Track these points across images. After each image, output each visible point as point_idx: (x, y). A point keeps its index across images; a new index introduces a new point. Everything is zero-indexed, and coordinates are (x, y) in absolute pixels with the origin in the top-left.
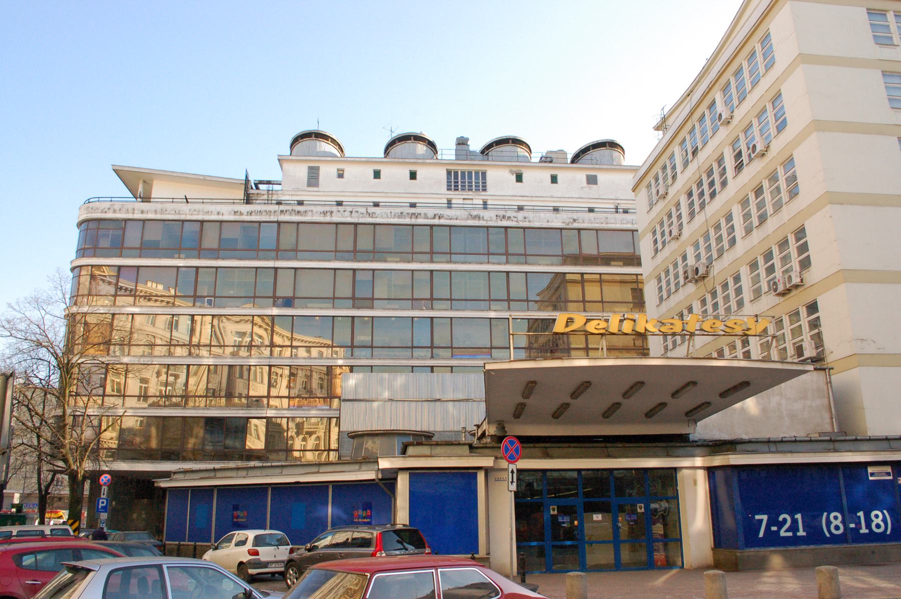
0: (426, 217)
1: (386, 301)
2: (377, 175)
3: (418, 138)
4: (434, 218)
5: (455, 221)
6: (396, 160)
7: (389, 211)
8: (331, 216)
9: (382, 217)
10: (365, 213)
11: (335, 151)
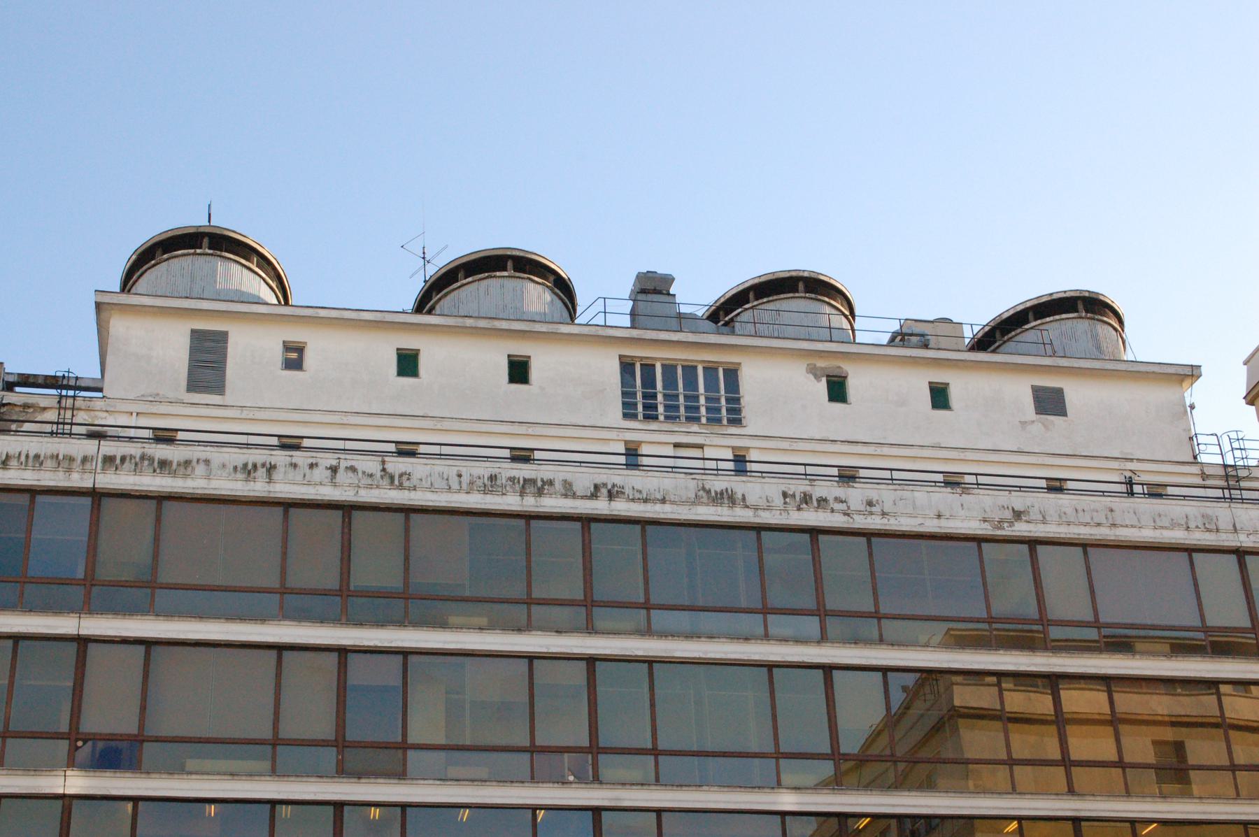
0: (568, 491)
1: (442, 754)
2: (408, 364)
3: (527, 266)
4: (594, 496)
5: (658, 507)
6: (469, 322)
7: (454, 471)
8: (270, 480)
9: (432, 488)
10: (379, 474)
11: (264, 290)
